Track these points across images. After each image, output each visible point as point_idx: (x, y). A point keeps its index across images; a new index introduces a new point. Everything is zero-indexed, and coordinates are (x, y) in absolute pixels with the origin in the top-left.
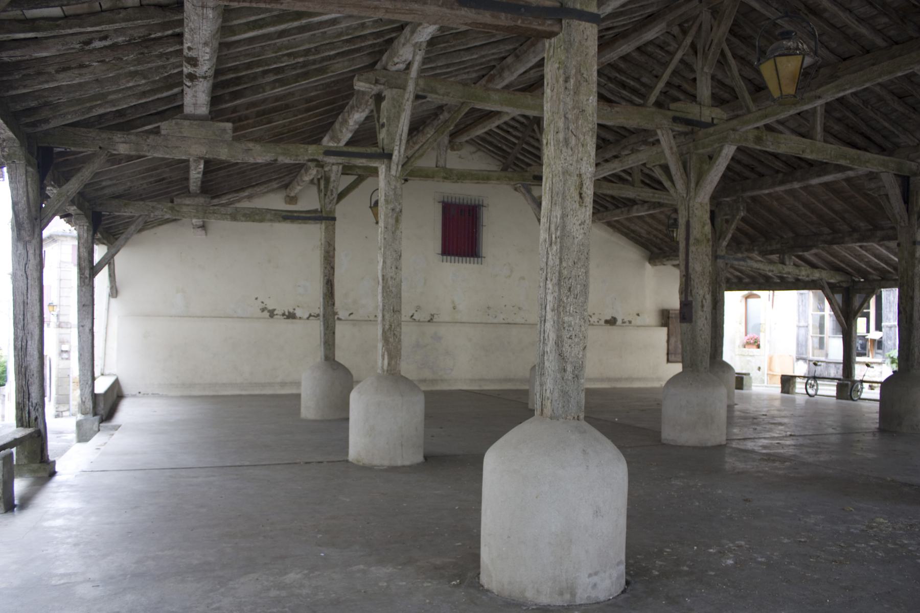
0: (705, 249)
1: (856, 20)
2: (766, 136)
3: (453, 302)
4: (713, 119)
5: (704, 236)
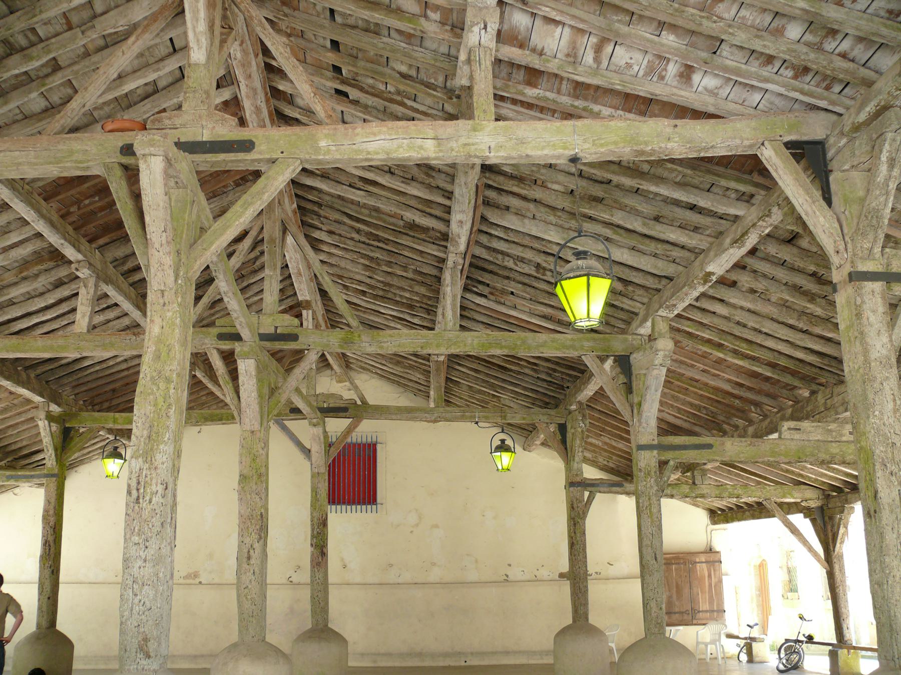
0: (254, 487)
1: (403, 182)
2: (359, 336)
3: (342, 560)
4: (276, 328)
5: (254, 471)
